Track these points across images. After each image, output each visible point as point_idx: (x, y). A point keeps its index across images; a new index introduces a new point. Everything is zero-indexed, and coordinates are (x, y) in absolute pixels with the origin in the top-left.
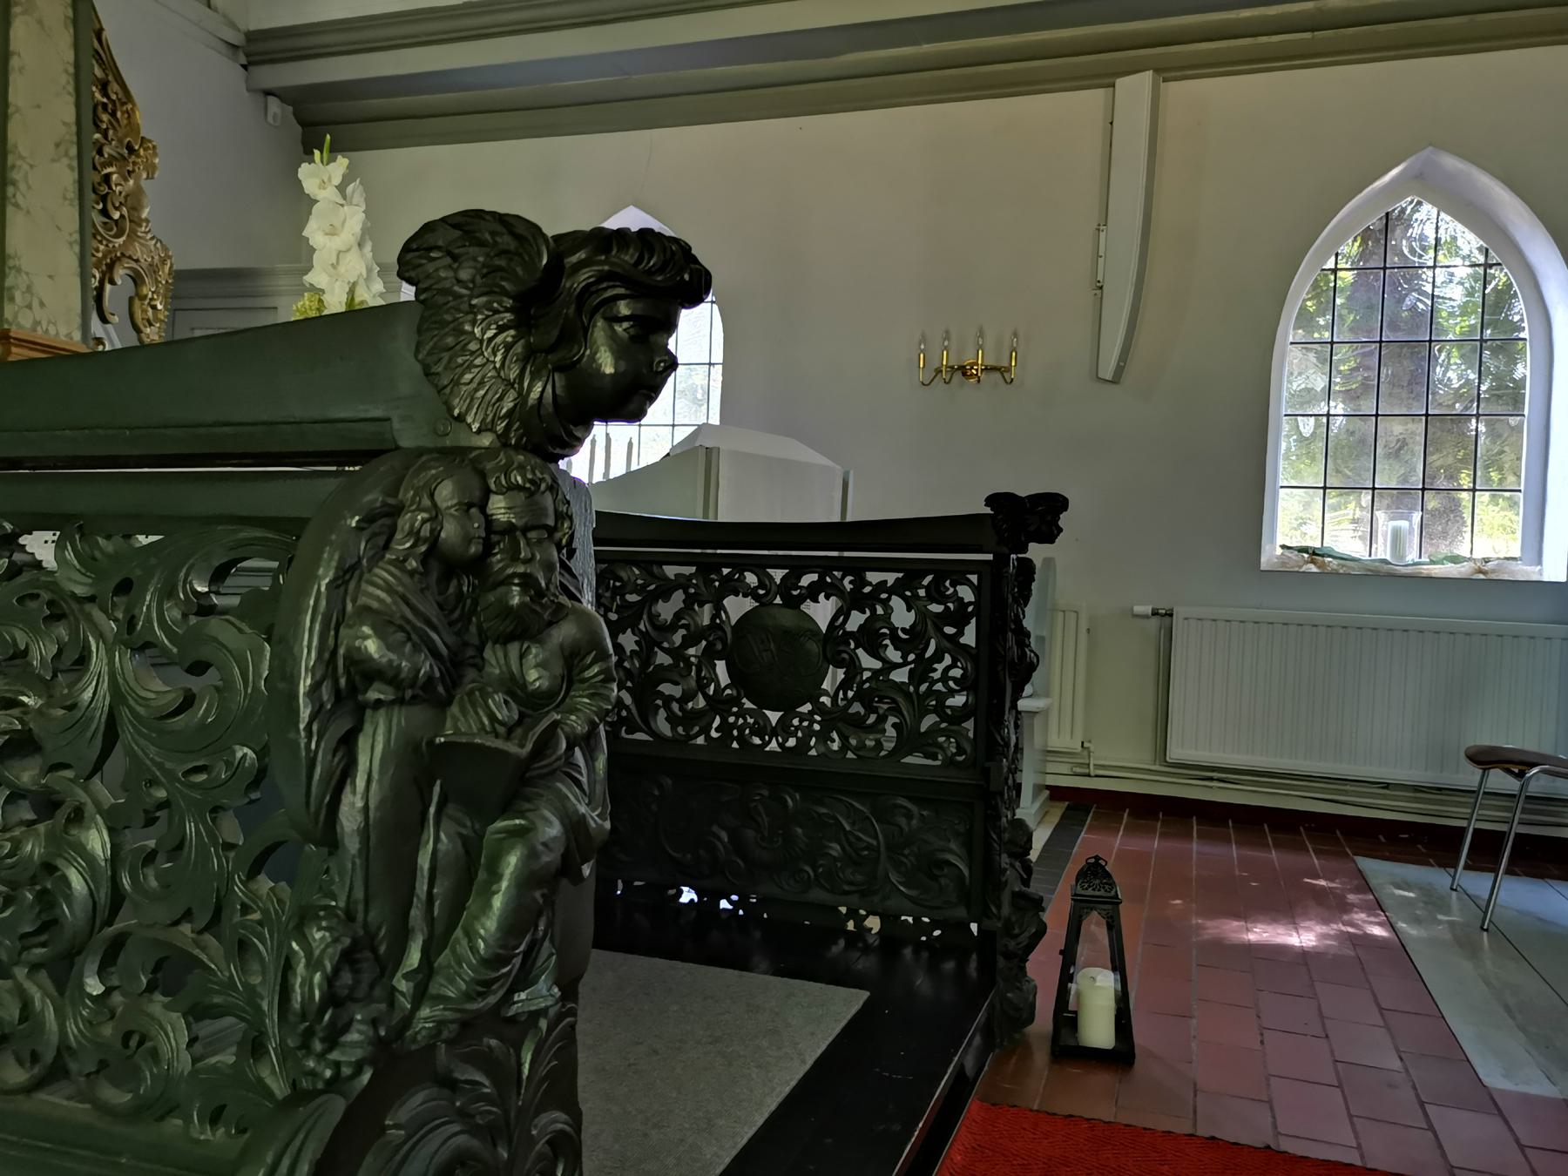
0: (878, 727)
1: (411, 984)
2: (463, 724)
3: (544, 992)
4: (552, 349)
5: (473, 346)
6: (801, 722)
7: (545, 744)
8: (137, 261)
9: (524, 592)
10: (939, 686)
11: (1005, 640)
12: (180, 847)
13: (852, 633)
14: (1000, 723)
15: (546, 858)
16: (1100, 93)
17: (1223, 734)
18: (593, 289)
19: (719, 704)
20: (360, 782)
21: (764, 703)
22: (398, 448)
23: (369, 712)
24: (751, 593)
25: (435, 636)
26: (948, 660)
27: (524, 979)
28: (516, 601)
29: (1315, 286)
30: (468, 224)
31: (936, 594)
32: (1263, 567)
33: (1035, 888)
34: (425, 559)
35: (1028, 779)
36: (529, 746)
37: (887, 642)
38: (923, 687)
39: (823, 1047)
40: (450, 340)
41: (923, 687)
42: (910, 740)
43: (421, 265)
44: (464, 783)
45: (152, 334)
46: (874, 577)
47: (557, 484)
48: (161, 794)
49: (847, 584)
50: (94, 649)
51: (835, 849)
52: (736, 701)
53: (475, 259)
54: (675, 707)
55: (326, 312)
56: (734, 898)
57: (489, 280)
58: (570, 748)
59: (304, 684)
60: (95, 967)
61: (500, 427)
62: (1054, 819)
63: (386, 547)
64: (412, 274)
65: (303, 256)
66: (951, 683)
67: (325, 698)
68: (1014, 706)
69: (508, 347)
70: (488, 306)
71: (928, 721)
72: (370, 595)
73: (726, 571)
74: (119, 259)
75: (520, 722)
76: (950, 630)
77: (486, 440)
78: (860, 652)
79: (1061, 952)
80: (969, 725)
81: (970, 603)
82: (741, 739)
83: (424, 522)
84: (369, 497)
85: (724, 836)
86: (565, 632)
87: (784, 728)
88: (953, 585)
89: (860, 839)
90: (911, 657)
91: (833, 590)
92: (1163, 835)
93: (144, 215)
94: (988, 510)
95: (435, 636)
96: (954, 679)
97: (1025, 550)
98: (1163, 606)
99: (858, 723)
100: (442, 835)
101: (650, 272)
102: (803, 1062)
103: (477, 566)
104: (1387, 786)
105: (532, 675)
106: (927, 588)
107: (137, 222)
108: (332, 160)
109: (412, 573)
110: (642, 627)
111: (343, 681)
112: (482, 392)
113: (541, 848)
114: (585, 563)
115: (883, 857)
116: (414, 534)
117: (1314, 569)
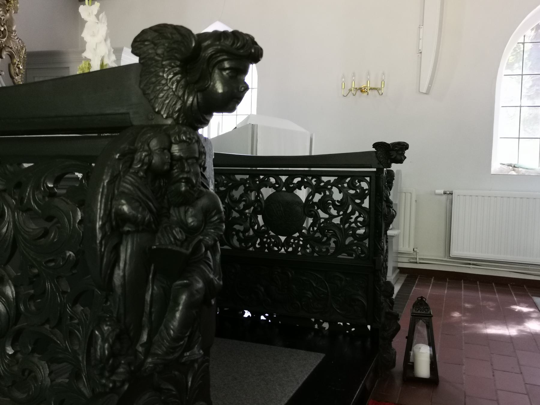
0: (327, 243)
1: (144, 349)
2: (172, 238)
3: (197, 352)
4: (197, 82)
5: (163, 82)
6: (294, 241)
7: (197, 248)
8: (11, 48)
10: (353, 225)
11: (382, 205)
14: (380, 241)
15: (198, 297)
18: (214, 56)
19: (259, 233)
20: (122, 265)
22: (132, 125)
23: (124, 236)
24: (272, 186)
25: (151, 204)
26: (357, 214)
27: (189, 347)
28: (183, 189)
29: (515, 50)
31: (352, 186)
33: (395, 310)
34: (146, 172)
35: (390, 265)
36: (190, 250)
37: (331, 206)
38: (347, 225)
39: (306, 377)
40: (154, 80)
41: (347, 225)
42: (341, 248)
43: (141, 48)
44: (165, 265)
45: (19, 79)
46: (325, 179)
47: (199, 140)
48: (36, 271)
49: (314, 182)
50: (6, 211)
51: (309, 294)
52: (267, 232)
53: (164, 45)
54: (241, 235)
55: (92, 70)
56: (267, 315)
58: (206, 251)
59: (99, 224)
60: (10, 342)
62: (402, 281)
63: (130, 166)
64: (138, 52)
65: (81, 46)
66: (359, 224)
67: (107, 230)
68: (386, 233)
69: (178, 82)
70: (169, 64)
72: (125, 187)
73: (261, 177)
74: (3, 48)
75: (186, 240)
76: (358, 201)
77: (169, 122)
78: (319, 211)
79: (407, 337)
80: (367, 241)
81: (366, 190)
82: (269, 248)
83: (146, 156)
84: (123, 146)
85: (262, 289)
86: (203, 202)
87: (287, 244)
88: (359, 182)
90: (341, 213)
91: (307, 185)
93: (14, 28)
95: (151, 204)
96: (360, 222)
97: (390, 167)
98: (448, 190)
99: (318, 241)
100: (155, 287)
101: (238, 49)
102: (298, 383)
103: (166, 175)
105: (190, 220)
106: (348, 183)
107: (11, 32)
108: (93, 4)
109: (141, 178)
110: (226, 201)
111: (114, 223)
112: (167, 101)
113: (195, 292)
114: (210, 172)
116: (141, 161)
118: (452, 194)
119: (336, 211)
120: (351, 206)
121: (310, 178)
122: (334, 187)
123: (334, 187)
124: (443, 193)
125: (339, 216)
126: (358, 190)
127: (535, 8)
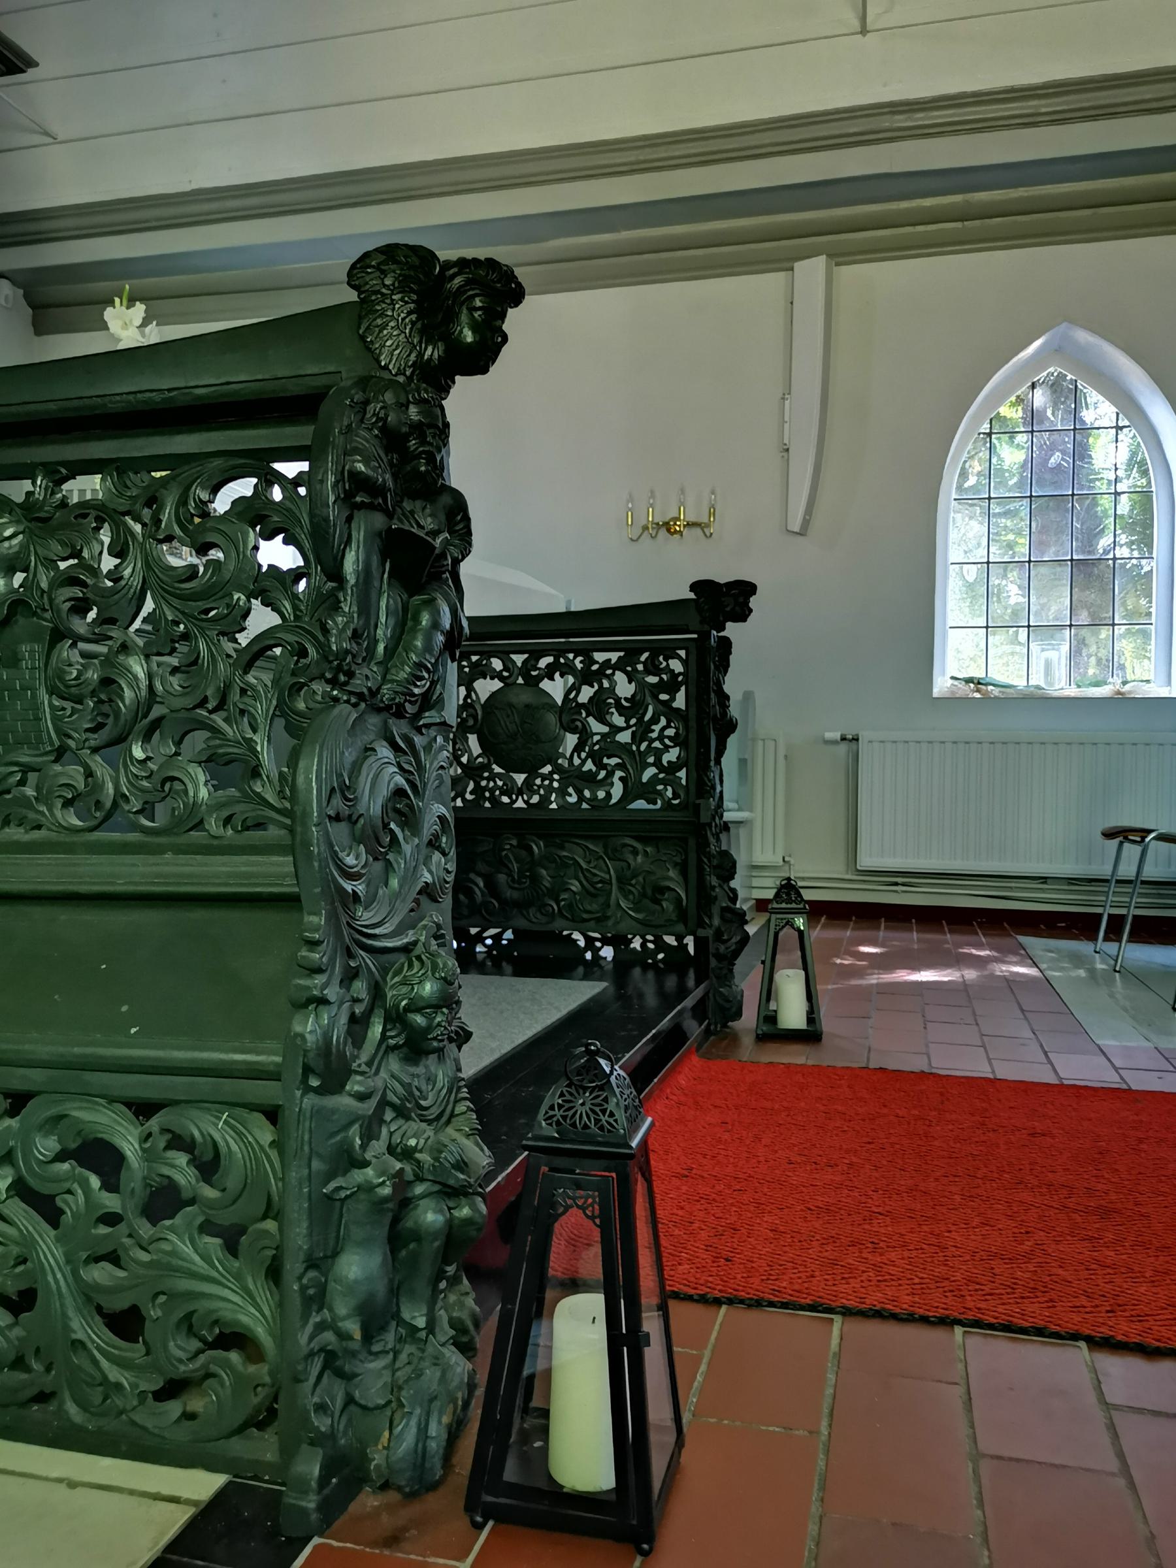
0: (607, 782)
6: (542, 781)
9: (427, 464)
10: (657, 744)
11: (709, 698)
12: (195, 662)
13: (583, 704)
16: (781, 275)
17: (907, 838)
21: (511, 766)
24: (497, 675)
26: (663, 721)
30: (390, 252)
32: (935, 695)
37: (613, 710)
38: (643, 746)
40: (379, 321)
41: (643, 746)
42: (633, 790)
46: (600, 657)
52: (487, 767)
57: (403, 286)
61: (408, 373)
63: (362, 421)
66: (667, 741)
69: (413, 323)
70: (402, 300)
71: (650, 772)
73: (474, 658)
76: (664, 697)
78: (591, 720)
80: (682, 774)
81: (680, 674)
83: (381, 408)
88: (666, 659)
89: (595, 875)
90: (633, 721)
92: (853, 929)
94: (692, 596)
96: (669, 737)
97: (723, 629)
99: (590, 779)
104: (1044, 880)
106: (644, 663)
115: (614, 888)
117: (977, 695)
118: (857, 740)
119: (623, 719)
120: (650, 708)
121: (571, 656)
122: (617, 673)
123: (617, 673)
124: (839, 738)
125: (628, 727)
126: (664, 677)
127: (1007, 362)
